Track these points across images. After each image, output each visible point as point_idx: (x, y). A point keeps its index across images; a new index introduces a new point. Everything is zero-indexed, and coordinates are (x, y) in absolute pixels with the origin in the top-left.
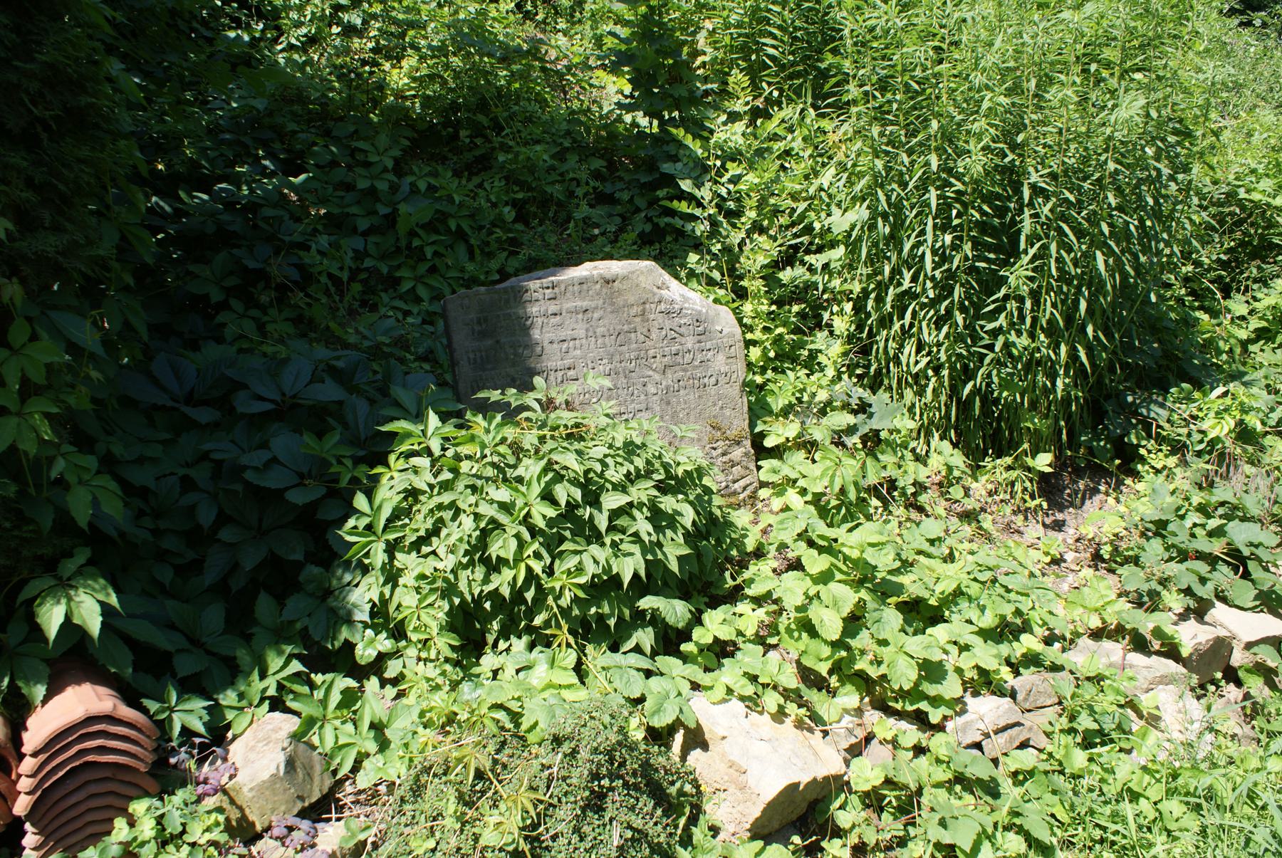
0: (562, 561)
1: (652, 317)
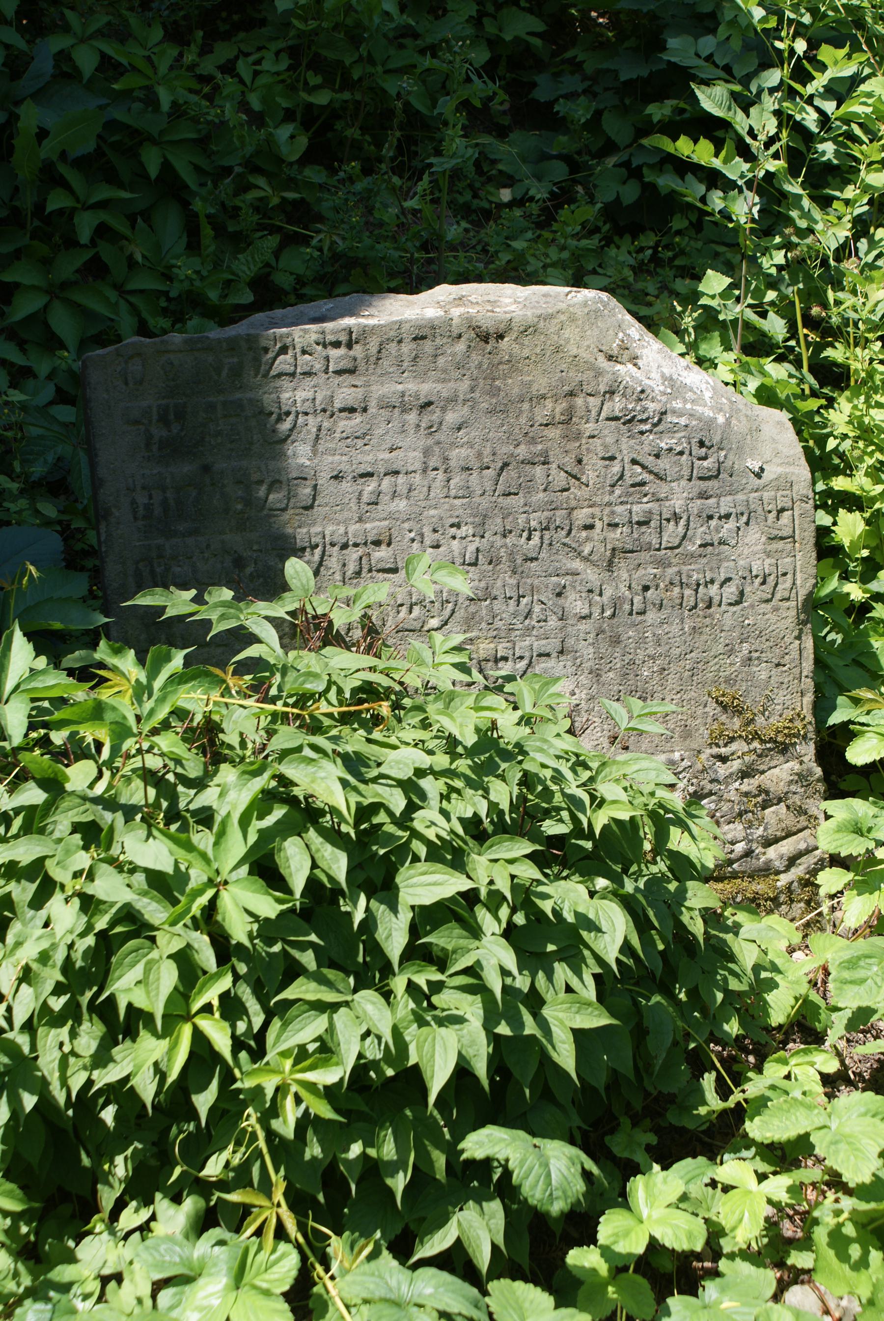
0: (285, 1025)
1: (590, 428)
